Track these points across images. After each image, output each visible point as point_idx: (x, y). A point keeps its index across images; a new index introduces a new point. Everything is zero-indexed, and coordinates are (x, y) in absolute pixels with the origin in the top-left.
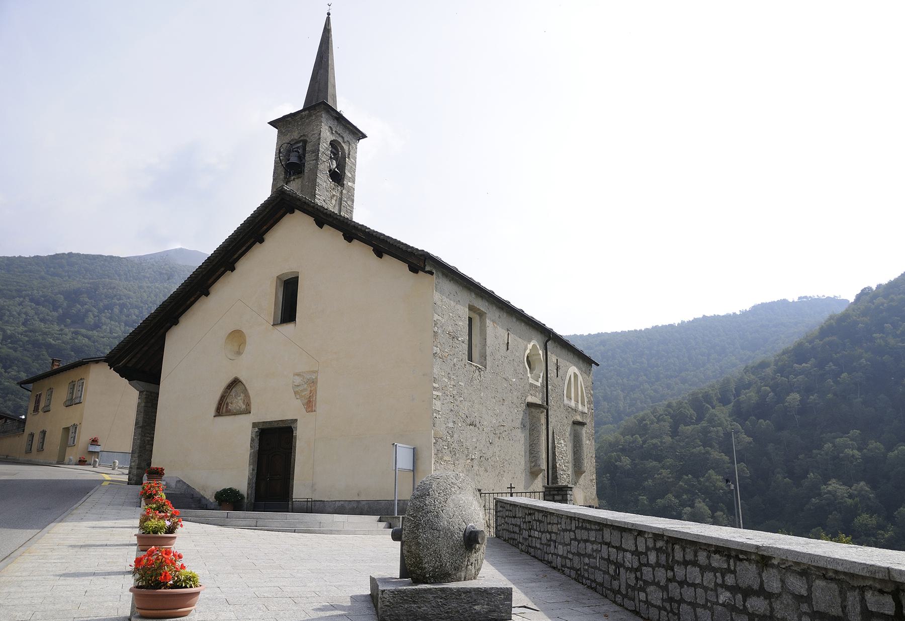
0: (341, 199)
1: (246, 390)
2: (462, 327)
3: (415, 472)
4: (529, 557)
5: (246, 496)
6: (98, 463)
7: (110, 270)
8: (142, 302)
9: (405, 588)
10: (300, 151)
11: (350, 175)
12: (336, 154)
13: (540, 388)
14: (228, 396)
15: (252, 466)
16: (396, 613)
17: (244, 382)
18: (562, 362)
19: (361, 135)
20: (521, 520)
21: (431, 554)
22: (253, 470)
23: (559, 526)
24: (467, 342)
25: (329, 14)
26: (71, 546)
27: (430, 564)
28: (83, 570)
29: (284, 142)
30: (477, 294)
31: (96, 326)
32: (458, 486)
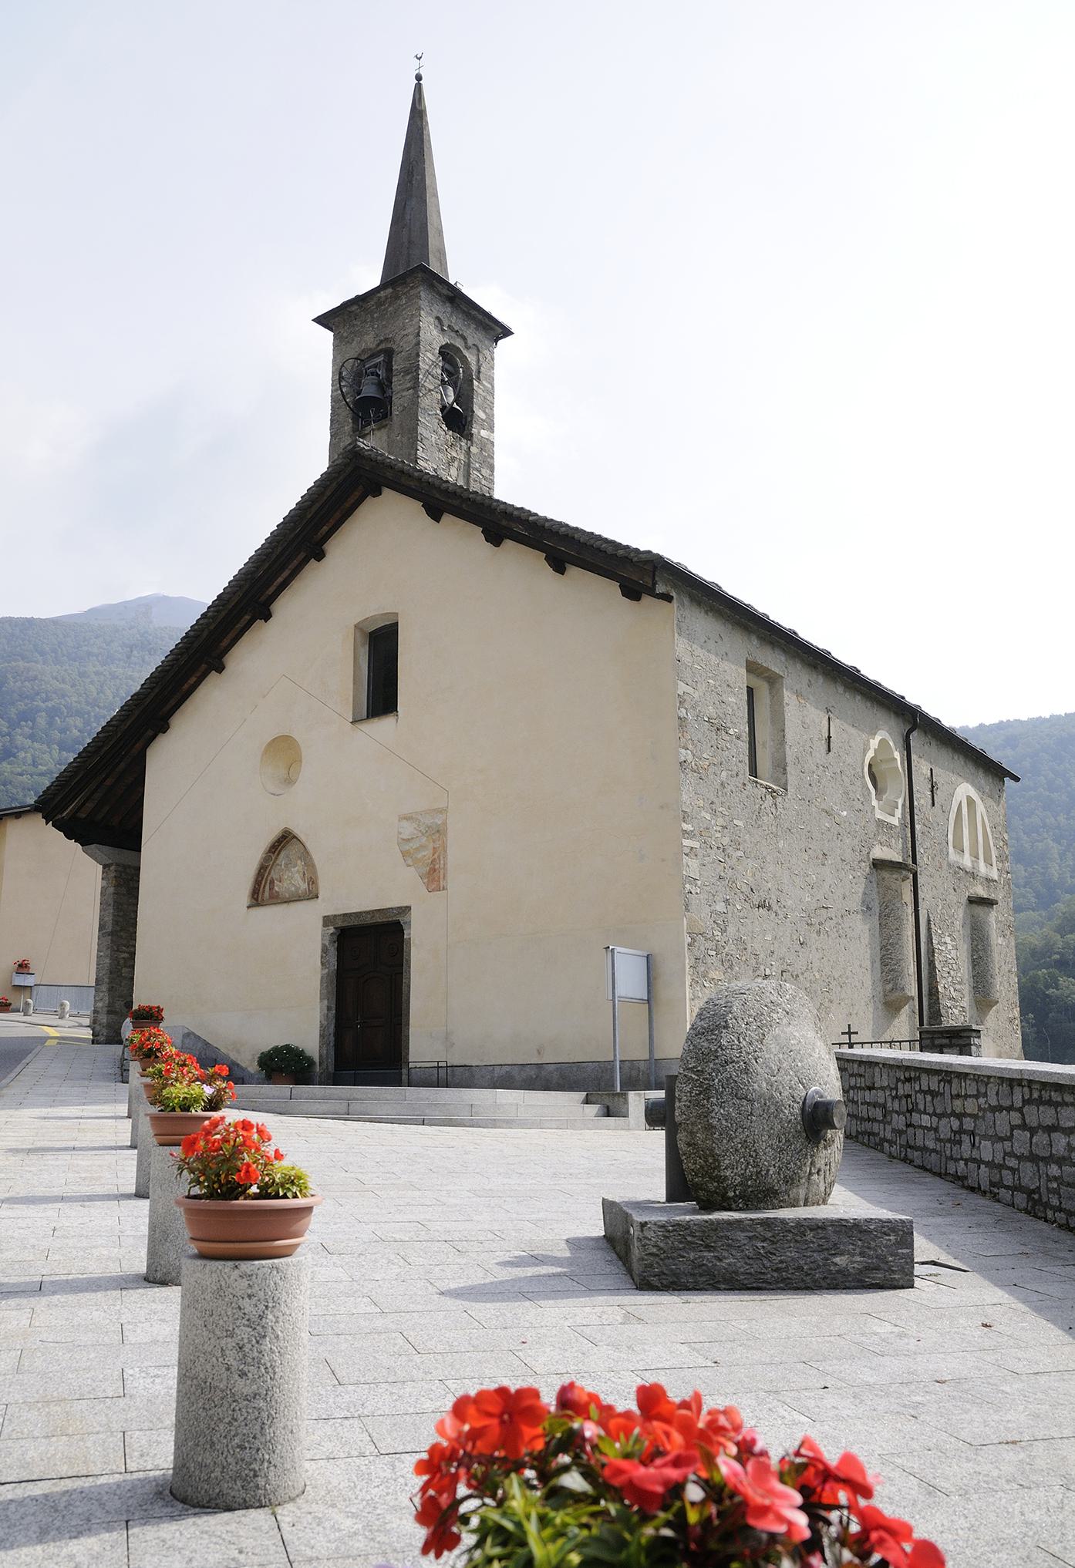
0: (468, 465)
1: (308, 853)
2: (735, 708)
3: (652, 1003)
4: (911, 1169)
5: (317, 1059)
6: (32, 1008)
7: (24, 645)
8: (87, 703)
9: (688, 1218)
10: (379, 373)
11: (482, 415)
12: (453, 375)
13: (898, 830)
14: (272, 867)
15: (326, 1002)
16: (672, 1270)
17: (302, 837)
18: (940, 777)
19: (501, 331)
20: (888, 1093)
21: (736, 1150)
22: (329, 1009)
23: (982, 1100)
24: (745, 737)
25: (419, 78)
26: (10, 1150)
27: (735, 1171)
28: (40, 1191)
29: (348, 356)
30: (762, 639)
32: (784, 1010)
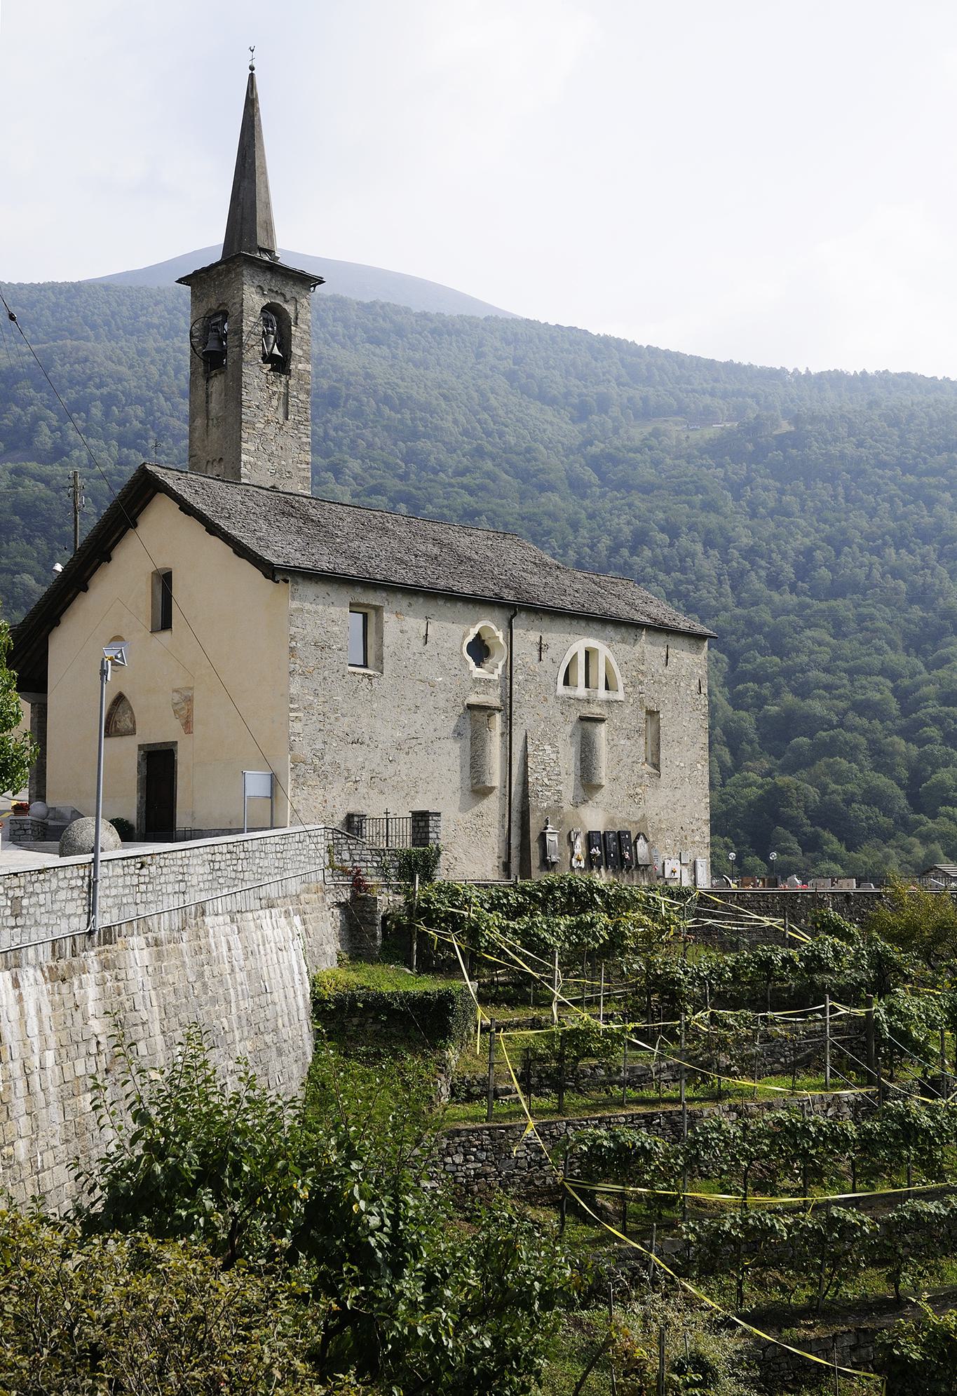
0: (287, 395)
7: (71, 317)
11: (300, 352)
22: (141, 797)
25: (252, 68)
31: (59, 453)
